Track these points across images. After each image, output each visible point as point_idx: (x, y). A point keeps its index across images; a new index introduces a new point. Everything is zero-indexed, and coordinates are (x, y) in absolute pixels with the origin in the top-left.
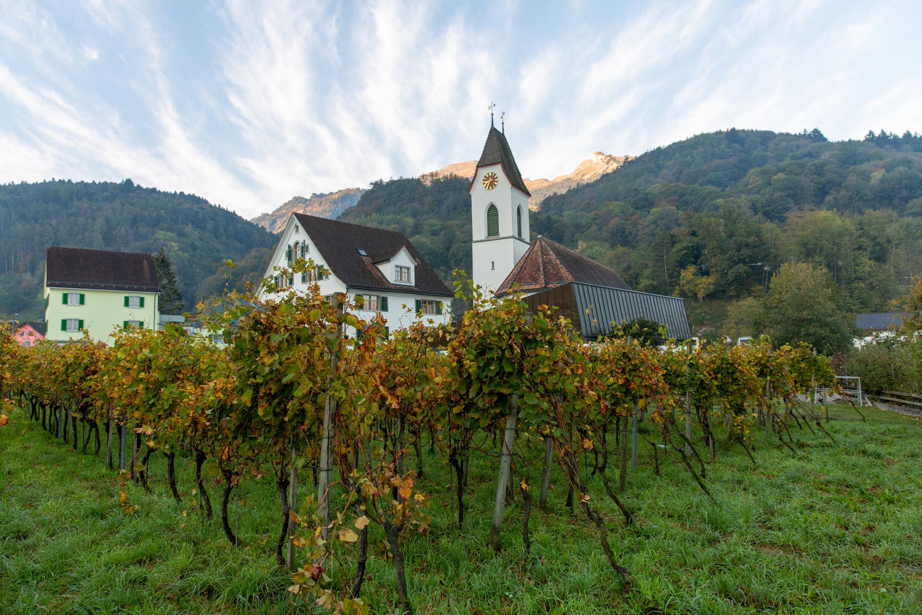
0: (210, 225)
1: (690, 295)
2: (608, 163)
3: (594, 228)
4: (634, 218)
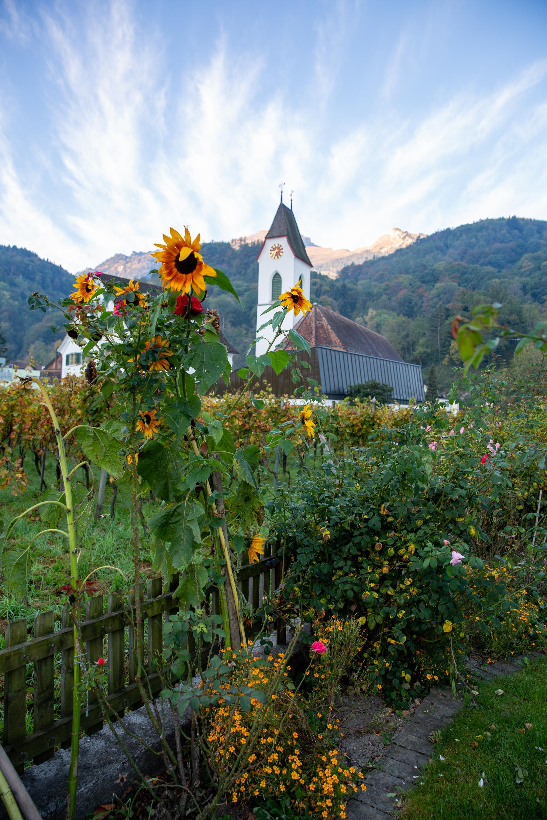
0: (38, 277)
1: (457, 363)
2: (404, 238)
3: (384, 297)
4: (420, 291)
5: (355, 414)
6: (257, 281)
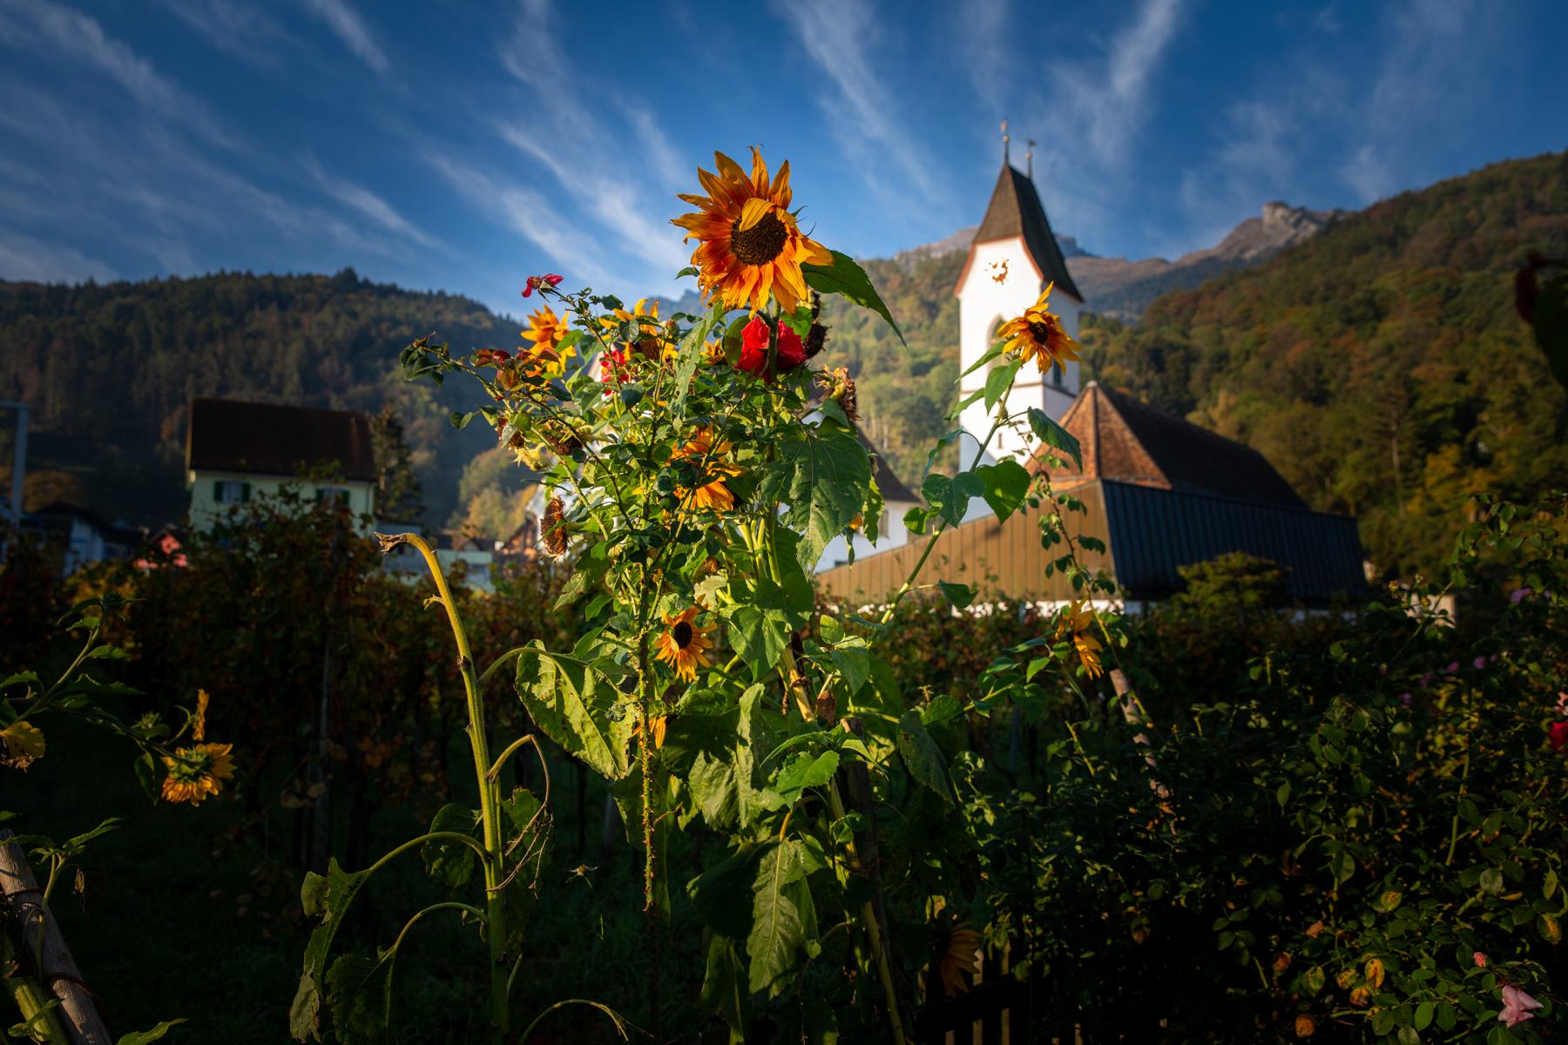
2: (1297, 224)
6: (957, 341)
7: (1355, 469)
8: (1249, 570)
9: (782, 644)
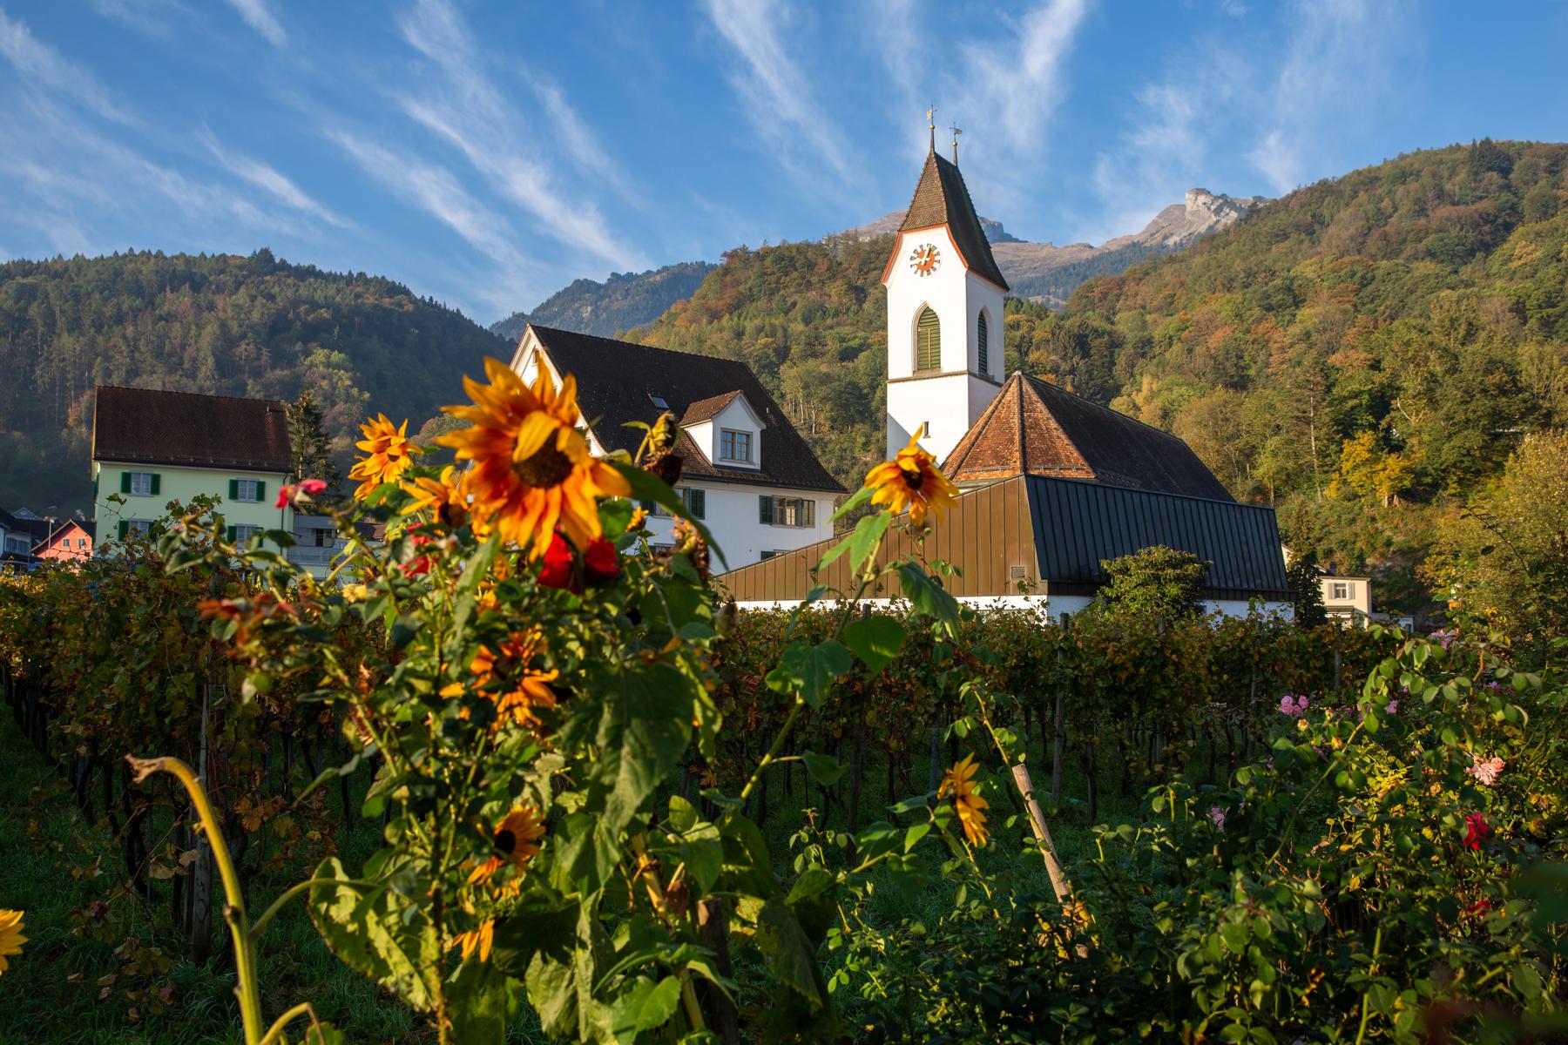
2: (1218, 211)
4: (1261, 329)
5: (1119, 641)
6: (884, 327)
7: (1275, 454)
8: (1171, 563)
9: (616, 856)
